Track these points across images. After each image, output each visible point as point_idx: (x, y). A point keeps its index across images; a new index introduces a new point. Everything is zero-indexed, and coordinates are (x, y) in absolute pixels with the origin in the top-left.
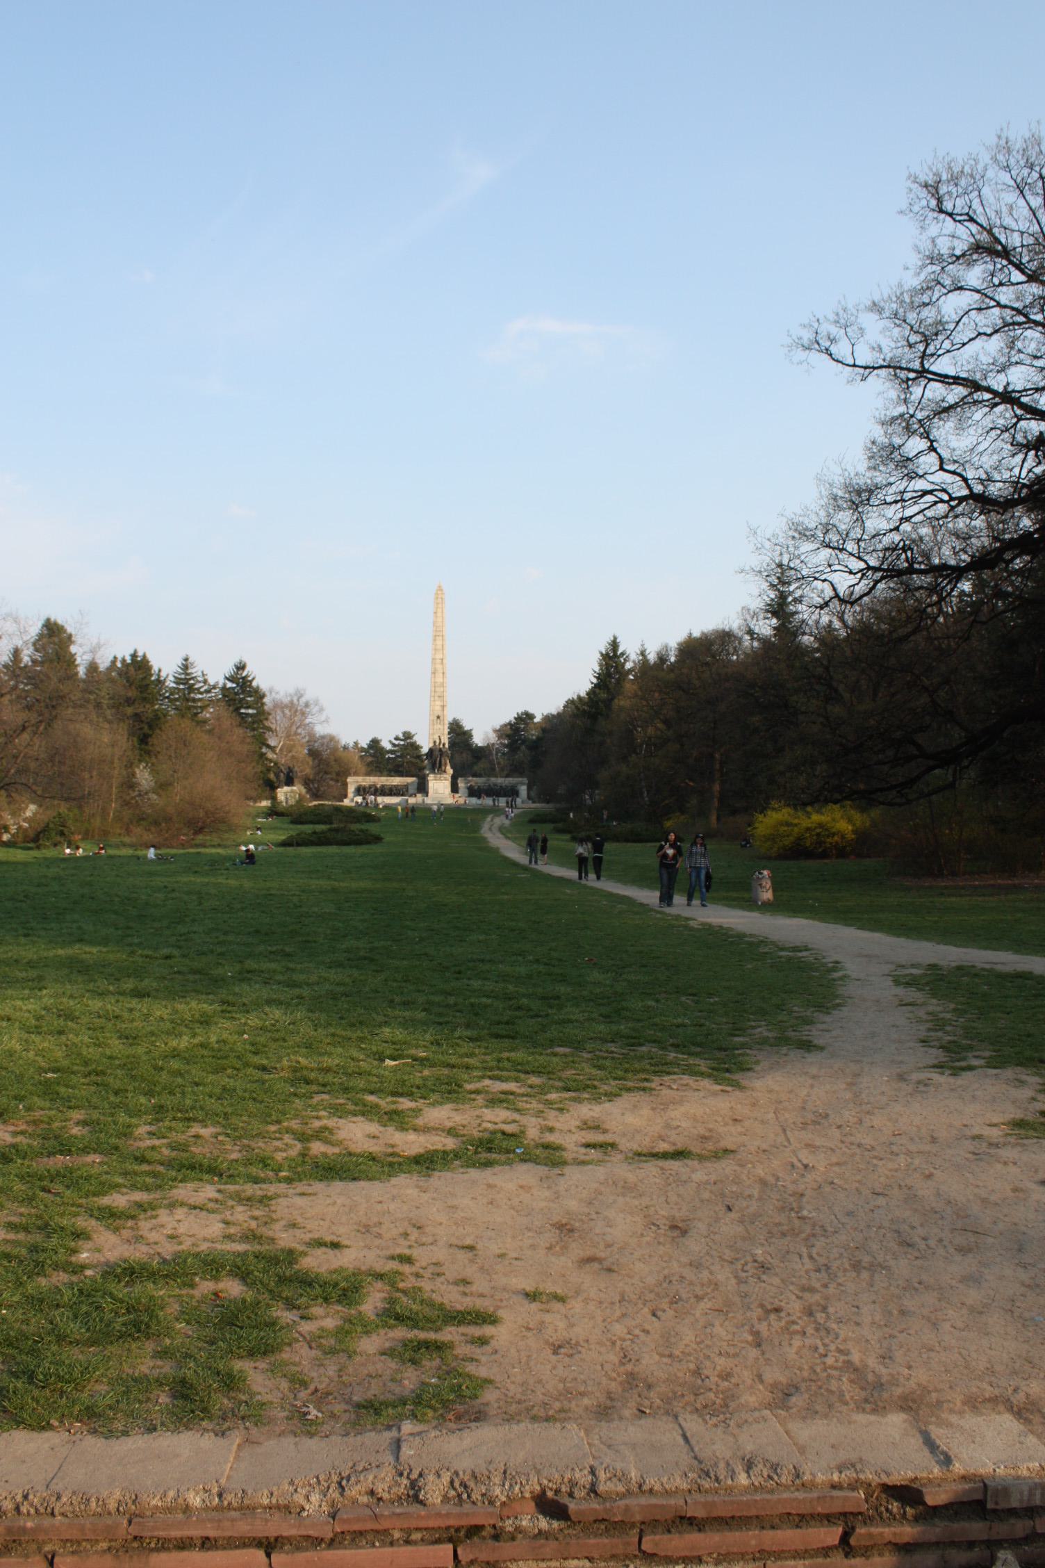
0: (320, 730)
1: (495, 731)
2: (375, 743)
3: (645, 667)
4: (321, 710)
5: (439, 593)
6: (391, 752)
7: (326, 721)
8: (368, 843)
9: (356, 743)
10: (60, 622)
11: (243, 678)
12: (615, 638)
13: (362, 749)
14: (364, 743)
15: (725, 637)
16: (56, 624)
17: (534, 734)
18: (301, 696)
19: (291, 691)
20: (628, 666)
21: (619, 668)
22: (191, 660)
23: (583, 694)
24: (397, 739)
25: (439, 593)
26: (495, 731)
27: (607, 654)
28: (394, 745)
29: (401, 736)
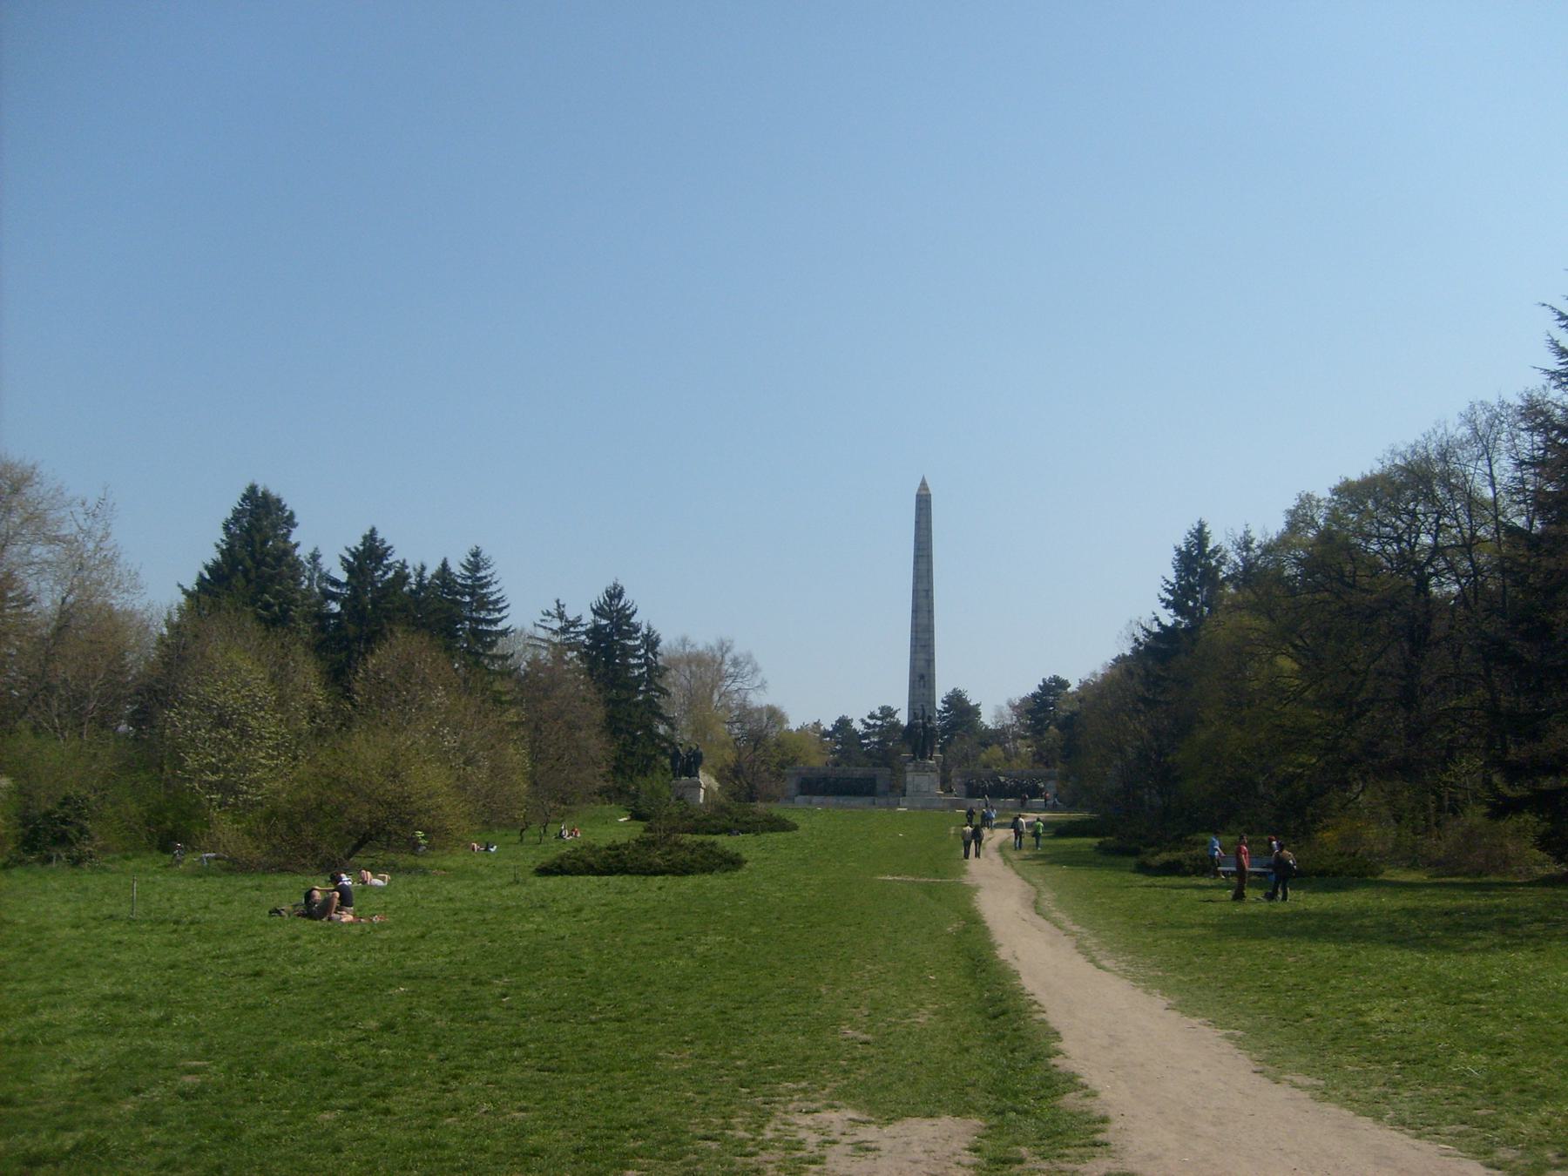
0: (758, 700)
1: (1014, 707)
2: (843, 724)
3: (1249, 575)
4: (755, 670)
5: (923, 503)
6: (866, 736)
7: (762, 686)
8: (709, 870)
9: (817, 724)
10: (274, 491)
11: (618, 611)
12: (1202, 526)
13: (826, 734)
14: (828, 725)
15: (1417, 482)
16: (266, 495)
17: (1065, 709)
18: (728, 649)
19: (713, 643)
20: (1225, 571)
21: (1209, 575)
22: (484, 555)
23: (1128, 653)
24: (872, 716)
25: (923, 503)
26: (1014, 707)
27: (1189, 552)
28: (868, 726)
29: (877, 713)
